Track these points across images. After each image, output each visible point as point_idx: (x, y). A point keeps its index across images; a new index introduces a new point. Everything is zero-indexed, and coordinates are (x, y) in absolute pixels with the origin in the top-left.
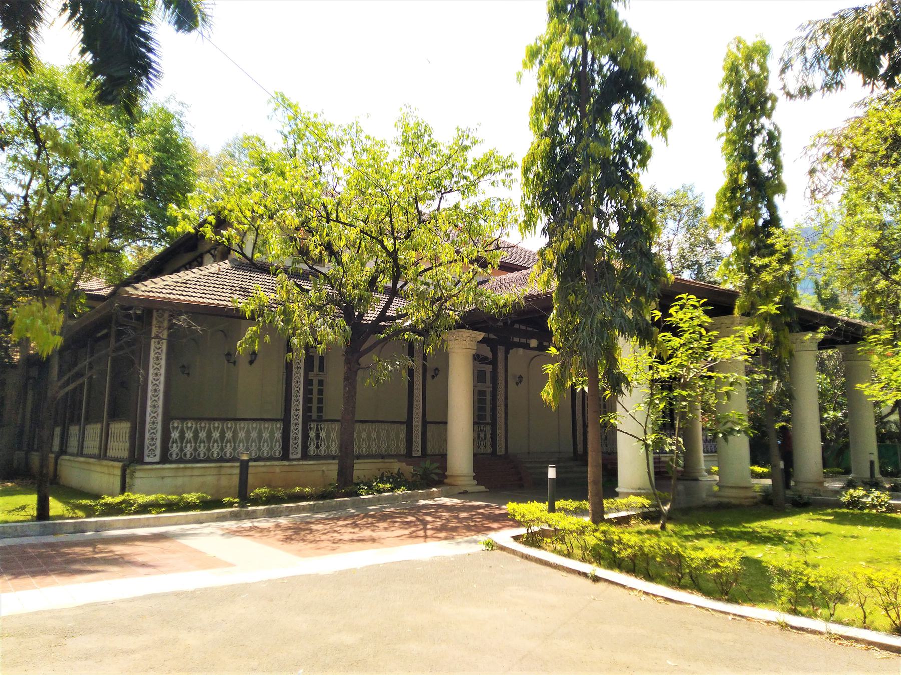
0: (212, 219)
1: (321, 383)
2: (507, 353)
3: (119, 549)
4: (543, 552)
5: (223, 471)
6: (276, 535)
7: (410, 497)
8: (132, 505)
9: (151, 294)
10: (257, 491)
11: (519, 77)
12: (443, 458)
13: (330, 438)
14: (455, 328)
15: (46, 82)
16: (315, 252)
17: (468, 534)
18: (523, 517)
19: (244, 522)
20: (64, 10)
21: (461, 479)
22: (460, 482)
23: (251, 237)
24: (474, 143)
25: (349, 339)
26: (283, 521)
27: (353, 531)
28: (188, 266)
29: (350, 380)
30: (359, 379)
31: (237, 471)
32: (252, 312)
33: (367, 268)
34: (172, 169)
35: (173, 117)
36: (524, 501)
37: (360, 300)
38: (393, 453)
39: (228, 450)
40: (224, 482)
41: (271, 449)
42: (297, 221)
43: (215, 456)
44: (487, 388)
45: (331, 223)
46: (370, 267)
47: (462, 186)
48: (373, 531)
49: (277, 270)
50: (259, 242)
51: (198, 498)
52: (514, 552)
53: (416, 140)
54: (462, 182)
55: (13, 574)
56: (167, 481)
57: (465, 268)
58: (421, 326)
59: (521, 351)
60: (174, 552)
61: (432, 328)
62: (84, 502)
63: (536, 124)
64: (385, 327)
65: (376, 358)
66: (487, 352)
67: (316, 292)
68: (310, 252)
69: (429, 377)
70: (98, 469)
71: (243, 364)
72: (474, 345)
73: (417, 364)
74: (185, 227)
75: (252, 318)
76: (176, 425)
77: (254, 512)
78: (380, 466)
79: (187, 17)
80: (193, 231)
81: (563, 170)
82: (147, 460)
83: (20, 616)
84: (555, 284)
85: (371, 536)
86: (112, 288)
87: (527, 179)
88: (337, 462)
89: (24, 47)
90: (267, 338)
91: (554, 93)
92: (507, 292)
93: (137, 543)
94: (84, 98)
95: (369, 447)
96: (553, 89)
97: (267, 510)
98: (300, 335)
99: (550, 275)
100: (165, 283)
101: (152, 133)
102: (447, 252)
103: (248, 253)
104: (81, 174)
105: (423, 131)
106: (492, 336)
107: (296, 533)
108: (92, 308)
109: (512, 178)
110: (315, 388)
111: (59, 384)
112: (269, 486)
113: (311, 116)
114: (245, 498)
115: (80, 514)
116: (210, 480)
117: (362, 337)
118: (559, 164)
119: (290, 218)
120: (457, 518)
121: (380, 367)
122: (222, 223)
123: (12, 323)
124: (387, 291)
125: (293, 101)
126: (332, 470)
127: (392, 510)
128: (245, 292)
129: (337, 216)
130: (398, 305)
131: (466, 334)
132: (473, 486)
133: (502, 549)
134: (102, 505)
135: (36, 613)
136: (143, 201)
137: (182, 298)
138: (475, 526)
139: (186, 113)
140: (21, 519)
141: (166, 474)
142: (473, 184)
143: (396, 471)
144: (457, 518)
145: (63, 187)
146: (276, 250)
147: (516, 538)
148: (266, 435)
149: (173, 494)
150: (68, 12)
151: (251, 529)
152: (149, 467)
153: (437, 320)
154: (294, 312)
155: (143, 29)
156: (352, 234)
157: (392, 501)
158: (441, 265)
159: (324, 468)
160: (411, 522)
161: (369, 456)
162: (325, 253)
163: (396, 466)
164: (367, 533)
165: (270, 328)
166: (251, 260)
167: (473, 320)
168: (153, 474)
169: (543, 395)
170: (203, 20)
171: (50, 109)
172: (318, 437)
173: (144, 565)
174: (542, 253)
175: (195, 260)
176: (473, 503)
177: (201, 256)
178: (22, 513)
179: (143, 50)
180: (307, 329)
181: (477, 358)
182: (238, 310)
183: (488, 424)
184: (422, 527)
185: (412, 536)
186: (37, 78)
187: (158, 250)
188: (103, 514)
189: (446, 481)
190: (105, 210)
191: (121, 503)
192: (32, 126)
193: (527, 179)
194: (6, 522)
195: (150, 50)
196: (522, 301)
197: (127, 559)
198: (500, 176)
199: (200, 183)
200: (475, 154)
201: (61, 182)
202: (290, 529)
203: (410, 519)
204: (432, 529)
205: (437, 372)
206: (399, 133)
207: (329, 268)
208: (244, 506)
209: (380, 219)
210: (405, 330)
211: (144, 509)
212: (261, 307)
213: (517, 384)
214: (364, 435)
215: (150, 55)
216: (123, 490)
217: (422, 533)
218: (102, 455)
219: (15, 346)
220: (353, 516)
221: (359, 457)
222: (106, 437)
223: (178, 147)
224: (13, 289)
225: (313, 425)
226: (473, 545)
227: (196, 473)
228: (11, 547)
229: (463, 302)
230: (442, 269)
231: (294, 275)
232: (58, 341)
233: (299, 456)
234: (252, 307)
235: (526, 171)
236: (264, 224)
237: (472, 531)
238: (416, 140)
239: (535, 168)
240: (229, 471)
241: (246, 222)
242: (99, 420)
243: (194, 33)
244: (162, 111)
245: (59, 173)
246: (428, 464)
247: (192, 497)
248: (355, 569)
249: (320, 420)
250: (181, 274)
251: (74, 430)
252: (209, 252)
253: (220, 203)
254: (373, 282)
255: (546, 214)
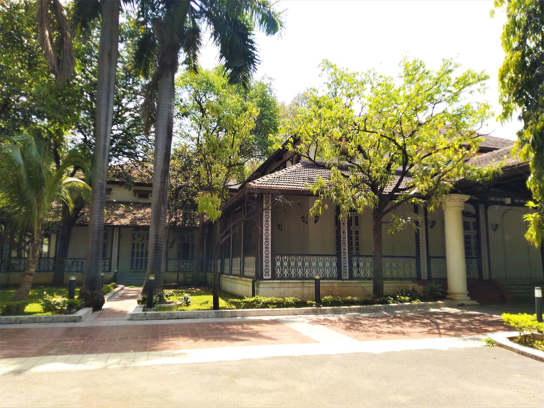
0: (291, 140)
1: (357, 233)
2: (486, 209)
3: (255, 328)
4: (536, 350)
5: (305, 285)
6: (340, 325)
7: (422, 306)
8: (259, 303)
9: (262, 185)
10: (326, 297)
11: (492, 13)
12: (444, 281)
13: (366, 267)
14: (450, 193)
15: (204, 78)
16: (351, 152)
17: (471, 333)
18: (517, 324)
19: (320, 315)
20: (211, 37)
21: (458, 295)
22: (458, 297)
23: (313, 148)
24: (456, 66)
25: (377, 203)
26: (343, 317)
27: (388, 326)
28: (278, 169)
29: (377, 229)
30: (383, 230)
31: (314, 285)
32: (317, 191)
33: (385, 159)
34: (267, 116)
35: (267, 87)
36: (516, 313)
37: (381, 179)
38: (408, 277)
39: (307, 272)
40: (306, 291)
41: (331, 272)
42: (340, 134)
43: (293, 276)
44: (473, 233)
45: (360, 133)
46: (386, 158)
47: (449, 97)
48: (402, 327)
49: (329, 165)
50: (318, 150)
51: (293, 300)
52: (511, 349)
53: (413, 72)
54: (448, 94)
55: (205, 339)
56: (276, 289)
57: (456, 151)
58: (425, 193)
59: (497, 207)
60: (284, 331)
61: (432, 194)
62: (236, 300)
63: (508, 44)
64: (397, 196)
65: (393, 216)
66: (471, 209)
67: (355, 176)
68: (348, 152)
69: (429, 228)
70: (240, 282)
71: (311, 223)
72: (462, 204)
73: (420, 218)
74: (277, 146)
75: (317, 195)
76: (278, 258)
77: (325, 310)
78: (400, 285)
79: (271, 24)
80: (281, 148)
81: (534, 72)
82: (265, 277)
83: (212, 363)
84: (532, 155)
85: (401, 331)
86: (240, 185)
87: (503, 83)
88: (372, 281)
89: (194, 61)
90: (326, 206)
91: (521, 19)
92: (488, 166)
93: (264, 325)
94: (222, 84)
95: (391, 273)
96: (521, 16)
97: (333, 309)
98: (346, 203)
99: (529, 149)
100: (269, 179)
101: (256, 97)
102: (442, 142)
103: (312, 156)
104: (223, 124)
105: (419, 65)
106: (474, 198)
107: (352, 325)
108: (231, 196)
109: (486, 86)
110: (354, 236)
111: (221, 236)
112: (332, 295)
113: (344, 70)
114: (319, 302)
115: (234, 307)
116: (298, 290)
117: (385, 204)
118: (529, 69)
119: (336, 133)
120: (460, 322)
121: (396, 221)
122: (297, 141)
123: (197, 205)
124: (397, 173)
125: (333, 63)
126: (369, 286)
127: (412, 314)
128: (311, 180)
129: (365, 128)
130: (407, 181)
131: (455, 196)
132: (467, 300)
133: (501, 346)
134: (244, 302)
135: (219, 362)
136: (253, 136)
137: (278, 186)
138: (475, 328)
139: (273, 83)
140: (206, 308)
141: (275, 285)
142: (456, 94)
143: (411, 289)
144: (460, 322)
145: (215, 133)
146: (328, 154)
147: (511, 339)
148: (327, 264)
149: (279, 297)
150: (213, 37)
151: (325, 320)
152: (266, 281)
153: (436, 188)
154: (342, 189)
155: (250, 37)
156: (374, 137)
157: (411, 308)
158: (438, 151)
159: (364, 285)
160: (427, 323)
161: (392, 279)
162: (357, 152)
163: (411, 286)
164: (398, 328)
165: (328, 200)
166: (314, 161)
167: (463, 187)
168: (268, 286)
169: (527, 236)
170: (281, 26)
171: (206, 92)
172: (358, 265)
173: (270, 338)
174: (520, 134)
175: (282, 164)
176: (470, 312)
177: (285, 162)
178: (207, 305)
179: (251, 50)
180: (350, 198)
181: (465, 214)
182: (309, 191)
183: (474, 258)
184: (436, 327)
185: (429, 332)
186: (200, 77)
187: (262, 162)
188: (245, 307)
189: (447, 296)
190: (238, 141)
191: (253, 301)
192: (199, 103)
193: (503, 83)
194: (199, 310)
195: (254, 49)
196: (501, 172)
197: (260, 333)
198: (474, 87)
199: (281, 121)
200: (455, 75)
201: (214, 131)
202: (348, 322)
203: (426, 321)
204: (443, 329)
205: (435, 224)
206: (402, 69)
207: (360, 161)
208: (319, 306)
209: (393, 126)
210: (412, 197)
211: (265, 305)
212: (322, 188)
213: (494, 230)
214: (388, 265)
215: (254, 52)
216: (253, 295)
217: (436, 331)
218: (242, 275)
219: (198, 217)
220: (385, 317)
221: (385, 279)
222: (243, 265)
223: (270, 103)
224: (195, 188)
225: (355, 259)
226: (477, 341)
227: (290, 285)
228: (203, 323)
229: (457, 174)
230: (439, 153)
231: (341, 168)
232: (220, 212)
233: (348, 277)
234: (317, 188)
235: (502, 77)
236: (320, 139)
237: (473, 331)
238: (413, 72)
239: (509, 74)
240: (308, 285)
241: (310, 139)
242: (229, 257)
243: (277, 34)
244: (261, 84)
245: (212, 126)
246: (433, 285)
247: (290, 300)
248: (396, 352)
249: (358, 255)
250: (276, 173)
251: (227, 261)
252: (289, 159)
253: (295, 130)
254: (389, 166)
255: (520, 105)
